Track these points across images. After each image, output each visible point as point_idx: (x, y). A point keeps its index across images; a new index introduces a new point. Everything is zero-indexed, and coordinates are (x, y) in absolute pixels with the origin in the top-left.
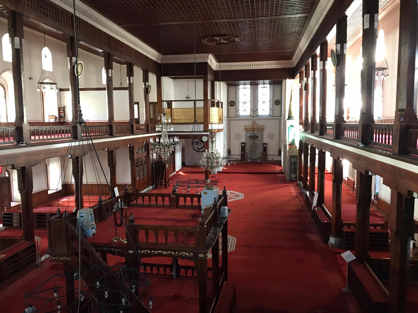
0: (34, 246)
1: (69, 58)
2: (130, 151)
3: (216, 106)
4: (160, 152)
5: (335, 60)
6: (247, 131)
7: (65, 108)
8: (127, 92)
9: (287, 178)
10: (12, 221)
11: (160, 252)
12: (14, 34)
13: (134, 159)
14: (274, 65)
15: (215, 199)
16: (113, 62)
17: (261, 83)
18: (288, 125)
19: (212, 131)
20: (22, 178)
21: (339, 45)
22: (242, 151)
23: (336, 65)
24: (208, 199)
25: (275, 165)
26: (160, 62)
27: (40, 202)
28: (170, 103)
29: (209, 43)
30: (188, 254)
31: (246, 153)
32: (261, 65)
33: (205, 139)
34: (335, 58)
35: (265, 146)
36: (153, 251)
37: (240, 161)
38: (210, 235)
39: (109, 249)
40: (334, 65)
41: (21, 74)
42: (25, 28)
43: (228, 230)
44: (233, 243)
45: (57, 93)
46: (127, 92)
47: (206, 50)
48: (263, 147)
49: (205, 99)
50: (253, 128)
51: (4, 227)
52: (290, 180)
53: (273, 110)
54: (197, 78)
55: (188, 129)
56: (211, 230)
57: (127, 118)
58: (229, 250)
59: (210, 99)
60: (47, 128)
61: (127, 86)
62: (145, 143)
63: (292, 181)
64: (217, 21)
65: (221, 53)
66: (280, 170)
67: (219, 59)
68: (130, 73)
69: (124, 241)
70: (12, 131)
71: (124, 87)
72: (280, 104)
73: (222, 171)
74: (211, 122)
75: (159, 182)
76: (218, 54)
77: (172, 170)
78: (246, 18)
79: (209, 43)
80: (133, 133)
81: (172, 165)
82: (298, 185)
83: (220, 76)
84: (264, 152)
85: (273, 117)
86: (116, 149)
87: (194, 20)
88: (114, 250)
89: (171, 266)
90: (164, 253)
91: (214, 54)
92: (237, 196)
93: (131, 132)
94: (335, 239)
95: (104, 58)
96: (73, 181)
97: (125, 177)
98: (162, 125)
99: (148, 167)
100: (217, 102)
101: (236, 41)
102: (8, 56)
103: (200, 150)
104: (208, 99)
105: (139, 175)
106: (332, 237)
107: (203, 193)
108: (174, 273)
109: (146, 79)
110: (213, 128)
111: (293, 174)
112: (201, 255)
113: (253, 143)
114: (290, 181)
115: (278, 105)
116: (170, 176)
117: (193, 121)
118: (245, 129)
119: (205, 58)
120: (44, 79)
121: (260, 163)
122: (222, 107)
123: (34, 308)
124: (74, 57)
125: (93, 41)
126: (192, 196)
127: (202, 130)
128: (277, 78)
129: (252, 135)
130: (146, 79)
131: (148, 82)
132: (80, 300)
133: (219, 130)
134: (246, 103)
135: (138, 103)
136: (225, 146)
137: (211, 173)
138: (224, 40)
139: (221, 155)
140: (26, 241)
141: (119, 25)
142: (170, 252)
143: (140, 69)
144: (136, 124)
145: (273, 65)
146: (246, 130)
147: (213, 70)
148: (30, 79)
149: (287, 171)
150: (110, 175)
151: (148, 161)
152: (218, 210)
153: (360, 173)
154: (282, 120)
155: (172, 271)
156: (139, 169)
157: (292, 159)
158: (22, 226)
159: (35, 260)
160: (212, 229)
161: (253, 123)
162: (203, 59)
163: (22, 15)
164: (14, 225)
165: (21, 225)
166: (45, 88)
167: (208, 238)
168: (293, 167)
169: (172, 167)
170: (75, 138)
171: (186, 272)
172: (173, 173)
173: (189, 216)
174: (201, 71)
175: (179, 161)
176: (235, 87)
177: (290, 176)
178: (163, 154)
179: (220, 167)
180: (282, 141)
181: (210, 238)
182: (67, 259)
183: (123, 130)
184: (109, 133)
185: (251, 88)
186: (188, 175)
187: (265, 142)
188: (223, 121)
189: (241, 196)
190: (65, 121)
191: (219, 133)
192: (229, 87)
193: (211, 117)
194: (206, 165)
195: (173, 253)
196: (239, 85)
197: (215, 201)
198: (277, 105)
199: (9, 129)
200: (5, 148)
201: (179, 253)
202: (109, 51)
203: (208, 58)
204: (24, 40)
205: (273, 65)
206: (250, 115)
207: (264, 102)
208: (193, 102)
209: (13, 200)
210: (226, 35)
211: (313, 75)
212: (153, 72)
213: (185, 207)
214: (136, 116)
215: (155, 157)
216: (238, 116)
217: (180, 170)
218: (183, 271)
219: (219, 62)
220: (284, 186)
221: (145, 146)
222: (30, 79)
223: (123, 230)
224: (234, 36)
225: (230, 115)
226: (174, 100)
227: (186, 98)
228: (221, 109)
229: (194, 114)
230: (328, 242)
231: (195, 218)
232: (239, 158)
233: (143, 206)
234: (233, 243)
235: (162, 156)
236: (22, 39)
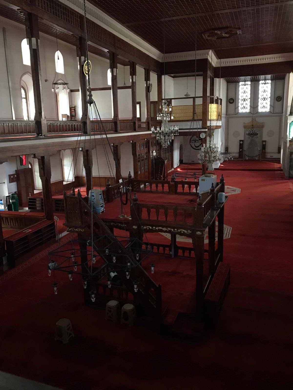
0: (53, 224)
1: (78, 57)
2: (133, 148)
3: (215, 102)
4: (161, 140)
8: (130, 90)
9: (286, 175)
10: (35, 205)
11: (160, 228)
12: (31, 35)
13: (136, 155)
15: (213, 184)
16: (118, 64)
17: (262, 79)
19: (210, 128)
20: (42, 166)
24: (205, 185)
25: (274, 163)
26: (161, 61)
27: (57, 191)
29: (209, 38)
30: (186, 231)
31: (244, 151)
33: (203, 136)
35: (264, 143)
36: (154, 227)
37: (237, 158)
38: (207, 216)
39: (116, 224)
41: (38, 73)
42: (40, 33)
43: (224, 220)
44: (228, 231)
45: (68, 93)
46: (130, 90)
47: (205, 46)
49: (204, 96)
51: (29, 210)
52: (289, 176)
53: (274, 107)
54: (197, 75)
55: (187, 126)
56: (208, 212)
57: (130, 116)
58: (225, 237)
59: (209, 95)
60: (61, 123)
61: (130, 84)
64: (219, 12)
65: (222, 49)
66: (279, 167)
67: (219, 56)
68: (133, 73)
69: (129, 218)
70: (33, 124)
71: (127, 86)
73: (219, 168)
74: (210, 119)
75: (158, 177)
76: (219, 49)
77: (170, 167)
78: (250, 6)
79: (209, 38)
80: (135, 130)
81: (170, 161)
83: (220, 72)
84: (263, 150)
85: (273, 113)
86: (121, 145)
87: (196, 13)
88: (120, 225)
89: (169, 247)
90: (164, 229)
91: (215, 50)
92: (233, 191)
93: (133, 129)
95: (109, 60)
96: (84, 174)
97: (128, 169)
98: (163, 114)
99: (148, 163)
100: (216, 99)
101: (238, 34)
102: (27, 60)
103: (197, 148)
104: (208, 95)
105: (141, 170)
107: (201, 180)
108: (172, 253)
109: (147, 78)
110: (212, 125)
112: (198, 233)
114: (289, 178)
115: (279, 101)
116: (168, 172)
117: (191, 118)
118: (244, 126)
119: (205, 55)
120: (58, 80)
121: (258, 160)
122: (221, 104)
123: (55, 263)
124: (83, 56)
126: (190, 184)
129: (251, 132)
130: (147, 78)
131: (150, 81)
132: (93, 262)
133: (218, 127)
134: (245, 100)
135: (139, 103)
136: (223, 143)
137: (208, 170)
138: (225, 33)
139: (219, 149)
140: (47, 220)
141: (123, 23)
142: (169, 229)
143: (142, 68)
144: (138, 121)
145: (276, 59)
146: (245, 127)
147: (213, 66)
148: (46, 81)
149: (286, 168)
150: (115, 168)
151: (148, 157)
152: (215, 195)
154: (284, 117)
155: (170, 250)
156: (140, 164)
158: (44, 210)
159: (55, 236)
160: (209, 212)
161: (252, 121)
162: (203, 55)
163: (38, 16)
164: (37, 208)
165: (43, 209)
166: (58, 88)
167: (205, 219)
169: (170, 163)
170: (85, 133)
171: (184, 252)
172: (171, 169)
173: (187, 201)
174: (200, 68)
176: (235, 83)
178: (163, 142)
179: (217, 162)
180: (283, 138)
181: (207, 219)
182: (81, 230)
183: (126, 127)
184: (114, 129)
185: (251, 85)
186: (186, 171)
187: (264, 139)
188: (222, 118)
189: (237, 191)
190: (76, 119)
191: (217, 130)
192: (228, 84)
193: (210, 114)
194: (203, 159)
195: (172, 230)
196: (239, 82)
197: (212, 186)
198: (278, 101)
200: (28, 139)
201: (177, 230)
202: (114, 50)
203: (208, 54)
205: (276, 59)
208: (192, 99)
209: (35, 188)
210: (227, 28)
212: (154, 71)
213: (183, 194)
214: (138, 116)
215: (155, 154)
216: (237, 114)
217: (178, 167)
218: (180, 251)
219: (219, 59)
220: (281, 183)
221: (146, 143)
222: (46, 81)
223: (127, 208)
224: (236, 28)
225: (229, 113)
226: (173, 98)
228: (220, 105)
229: (192, 111)
232: (237, 155)
233: (145, 192)
234: (228, 231)
235: (162, 144)
236: (38, 40)
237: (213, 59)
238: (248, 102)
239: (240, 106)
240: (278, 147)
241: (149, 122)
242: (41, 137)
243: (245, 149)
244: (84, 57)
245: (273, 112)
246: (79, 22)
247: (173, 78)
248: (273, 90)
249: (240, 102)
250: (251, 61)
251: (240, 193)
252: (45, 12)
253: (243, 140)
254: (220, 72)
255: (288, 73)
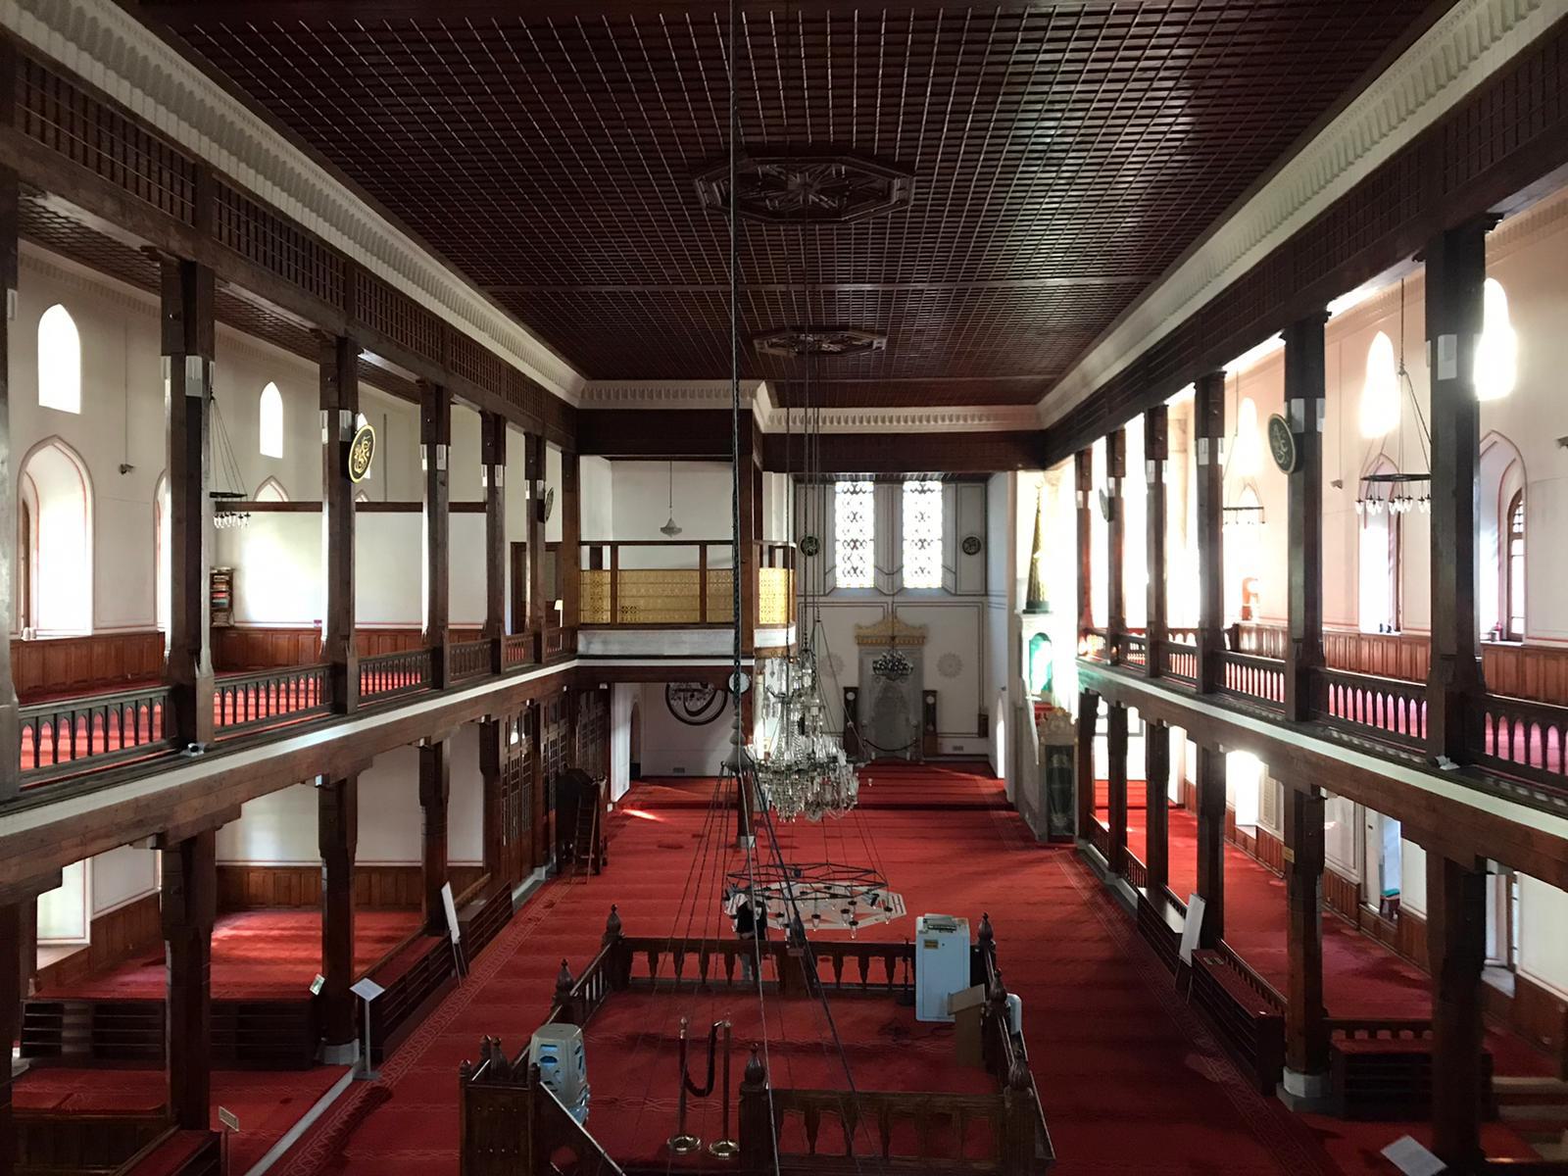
1: (326, 413)
5: (1289, 453)
6: (865, 644)
7: (235, 575)
8: (481, 519)
12: (186, 345)
14: (973, 420)
18: (1028, 634)
21: (1298, 405)
22: (846, 721)
23: (1292, 469)
26: (576, 404)
28: (596, 549)
32: (928, 421)
34: (1287, 444)
35: (930, 700)
40: (1284, 467)
46: (481, 519)
47: (752, 369)
48: (921, 705)
50: (893, 638)
53: (955, 573)
62: (528, 703)
63: (1055, 840)
66: (996, 794)
68: (436, 432)
72: (982, 551)
80: (496, 673)
82: (1080, 857)
83: (784, 453)
85: (955, 595)
93: (489, 667)
94: (1306, 1080)
106: (1294, 1070)
111: (1060, 815)
113: (886, 690)
114: (1050, 841)
121: (914, 763)
124: (195, 354)
125: (398, 346)
127: (729, 650)
128: (971, 467)
130: (535, 470)
134: (858, 544)
140: (182, 1128)
143: (519, 432)
146: (862, 641)
153: (1446, 859)
157: (1055, 759)
164: (66, 1049)
168: (1056, 786)
170: (337, 707)
175: (622, 763)
177: (1050, 821)
185: (876, 493)
187: (928, 686)
190: (232, 623)
199: (152, 696)
204: (16, 293)
206: (876, 589)
207: (922, 541)
211: (1153, 475)
219: (781, 406)
227: (663, 530)
230: (1278, 1090)
231: (909, 1042)
236: (211, 363)
237: (765, 410)
238: (868, 552)
239: (841, 566)
240: (980, 715)
241: (540, 635)
242: (194, 754)
243: (865, 722)
244: (350, 412)
245: (953, 592)
246: (341, 286)
247: (608, 462)
248: (951, 513)
249: (841, 551)
250: (880, 423)
251: (905, 913)
252: (240, 257)
253: (856, 688)
254: (784, 453)
255: (1004, 469)
